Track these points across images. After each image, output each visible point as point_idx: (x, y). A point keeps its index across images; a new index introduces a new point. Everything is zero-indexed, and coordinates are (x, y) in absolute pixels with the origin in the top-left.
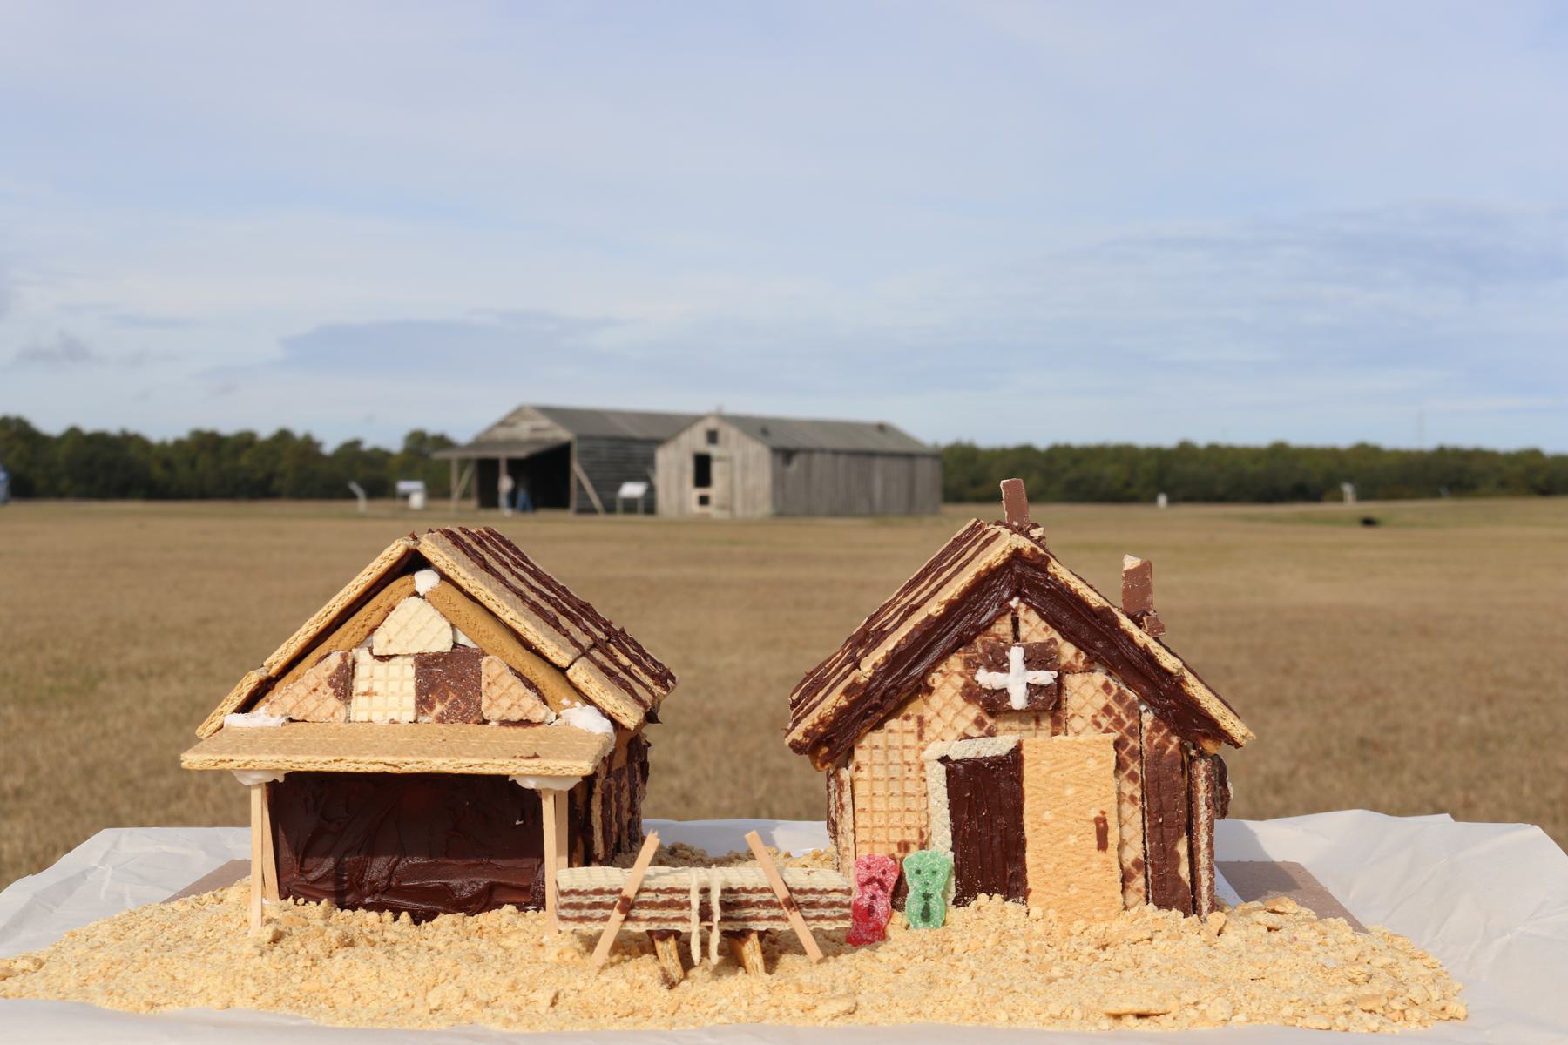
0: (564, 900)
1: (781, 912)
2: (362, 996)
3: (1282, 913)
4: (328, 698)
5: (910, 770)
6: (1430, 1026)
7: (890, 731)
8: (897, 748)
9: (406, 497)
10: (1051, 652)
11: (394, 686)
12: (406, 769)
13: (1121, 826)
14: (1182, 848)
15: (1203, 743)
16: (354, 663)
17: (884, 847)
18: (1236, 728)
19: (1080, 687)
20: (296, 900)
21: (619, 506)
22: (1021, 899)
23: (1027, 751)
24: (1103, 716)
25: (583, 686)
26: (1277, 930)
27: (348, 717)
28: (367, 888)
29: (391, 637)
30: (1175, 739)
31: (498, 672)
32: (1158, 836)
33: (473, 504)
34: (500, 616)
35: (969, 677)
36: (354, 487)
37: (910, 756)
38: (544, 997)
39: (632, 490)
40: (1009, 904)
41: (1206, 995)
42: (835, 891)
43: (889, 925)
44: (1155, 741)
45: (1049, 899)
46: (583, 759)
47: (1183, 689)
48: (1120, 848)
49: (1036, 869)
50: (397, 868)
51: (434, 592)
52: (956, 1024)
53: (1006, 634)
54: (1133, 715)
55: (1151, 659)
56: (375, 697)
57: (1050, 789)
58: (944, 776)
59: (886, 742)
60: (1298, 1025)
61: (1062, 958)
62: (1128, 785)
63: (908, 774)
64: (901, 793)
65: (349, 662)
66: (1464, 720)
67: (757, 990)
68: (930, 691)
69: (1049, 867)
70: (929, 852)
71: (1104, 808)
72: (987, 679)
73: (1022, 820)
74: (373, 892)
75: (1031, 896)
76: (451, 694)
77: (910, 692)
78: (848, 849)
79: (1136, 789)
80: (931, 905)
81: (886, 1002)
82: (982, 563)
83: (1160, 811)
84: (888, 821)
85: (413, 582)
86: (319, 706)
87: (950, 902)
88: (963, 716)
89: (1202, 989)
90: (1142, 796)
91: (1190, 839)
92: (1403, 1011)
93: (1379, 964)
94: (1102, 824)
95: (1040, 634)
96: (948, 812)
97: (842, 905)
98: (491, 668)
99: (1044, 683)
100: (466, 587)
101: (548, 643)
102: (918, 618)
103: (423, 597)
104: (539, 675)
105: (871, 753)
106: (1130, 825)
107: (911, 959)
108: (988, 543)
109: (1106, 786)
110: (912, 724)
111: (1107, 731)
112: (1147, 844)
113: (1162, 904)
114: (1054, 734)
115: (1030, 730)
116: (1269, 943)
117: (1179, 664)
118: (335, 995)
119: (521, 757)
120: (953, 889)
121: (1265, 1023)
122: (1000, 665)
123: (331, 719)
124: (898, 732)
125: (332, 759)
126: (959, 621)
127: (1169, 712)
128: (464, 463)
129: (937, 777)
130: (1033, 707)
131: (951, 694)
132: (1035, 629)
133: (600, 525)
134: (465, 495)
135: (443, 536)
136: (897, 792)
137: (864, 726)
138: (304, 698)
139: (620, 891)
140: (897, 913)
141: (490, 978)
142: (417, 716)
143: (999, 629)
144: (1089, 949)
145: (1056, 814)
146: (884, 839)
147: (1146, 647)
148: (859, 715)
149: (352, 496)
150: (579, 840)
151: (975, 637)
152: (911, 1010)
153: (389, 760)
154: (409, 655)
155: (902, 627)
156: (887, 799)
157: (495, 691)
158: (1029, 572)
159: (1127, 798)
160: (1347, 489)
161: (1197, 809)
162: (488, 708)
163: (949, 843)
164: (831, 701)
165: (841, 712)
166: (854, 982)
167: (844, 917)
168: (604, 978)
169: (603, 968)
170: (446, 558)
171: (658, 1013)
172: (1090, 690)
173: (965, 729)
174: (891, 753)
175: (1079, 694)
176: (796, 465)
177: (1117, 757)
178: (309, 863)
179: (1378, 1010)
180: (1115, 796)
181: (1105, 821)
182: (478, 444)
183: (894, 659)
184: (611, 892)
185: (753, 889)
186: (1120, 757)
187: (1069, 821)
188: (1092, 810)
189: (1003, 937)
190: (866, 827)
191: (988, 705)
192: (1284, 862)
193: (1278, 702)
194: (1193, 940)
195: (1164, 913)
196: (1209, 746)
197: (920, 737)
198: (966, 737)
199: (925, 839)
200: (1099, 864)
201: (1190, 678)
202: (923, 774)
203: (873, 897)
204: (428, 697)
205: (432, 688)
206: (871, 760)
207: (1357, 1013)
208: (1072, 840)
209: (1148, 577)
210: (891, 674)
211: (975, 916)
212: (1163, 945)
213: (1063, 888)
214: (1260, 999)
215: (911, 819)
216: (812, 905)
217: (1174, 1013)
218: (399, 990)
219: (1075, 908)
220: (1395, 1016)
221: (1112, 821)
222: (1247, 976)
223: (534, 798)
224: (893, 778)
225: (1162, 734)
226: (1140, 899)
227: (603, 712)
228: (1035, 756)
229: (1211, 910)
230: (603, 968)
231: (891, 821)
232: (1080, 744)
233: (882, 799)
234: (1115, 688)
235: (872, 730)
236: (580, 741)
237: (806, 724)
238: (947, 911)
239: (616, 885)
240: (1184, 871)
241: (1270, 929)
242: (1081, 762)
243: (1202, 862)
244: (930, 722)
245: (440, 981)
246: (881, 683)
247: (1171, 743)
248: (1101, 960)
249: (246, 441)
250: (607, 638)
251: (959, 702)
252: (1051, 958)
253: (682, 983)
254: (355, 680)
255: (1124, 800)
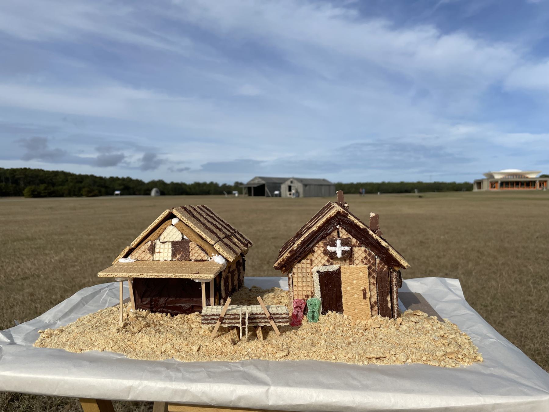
0: (203, 318)
1: (268, 320)
2: (144, 346)
3: (418, 315)
4: (148, 254)
5: (308, 274)
6: (472, 364)
7: (303, 263)
8: (305, 268)
9: (235, 194)
10: (349, 241)
11: (166, 250)
12: (161, 277)
13: (370, 292)
14: (389, 299)
15: (394, 268)
16: (155, 244)
17: (301, 296)
18: (405, 263)
19: (357, 251)
20: (140, 309)
21: (274, 195)
22: (341, 312)
23: (342, 270)
24: (365, 259)
25: (218, 250)
26: (418, 323)
27: (153, 259)
28: (159, 306)
29: (165, 237)
30: (386, 266)
31: (194, 246)
32: (381, 295)
33: (247, 195)
34: (195, 230)
35: (325, 248)
36: (225, 192)
37: (309, 270)
38: (195, 348)
39: (277, 192)
40: (337, 314)
41: (398, 352)
42: (284, 314)
43: (303, 320)
44: (380, 267)
45: (349, 313)
46: (211, 274)
47: (388, 252)
48: (370, 298)
49: (345, 304)
50: (167, 301)
51: (177, 224)
52: (319, 360)
53: (335, 236)
54: (373, 259)
55: (379, 243)
56: (161, 253)
57: (349, 281)
58: (318, 276)
59: (302, 266)
60: (428, 364)
61: (353, 334)
62: (372, 279)
63: (308, 276)
64: (306, 281)
65: (153, 244)
66: (442, 237)
67: (260, 346)
68: (314, 252)
69: (349, 303)
70: (314, 299)
71: (365, 287)
72: (329, 248)
73: (341, 289)
74: (161, 308)
75: (344, 312)
76: (181, 252)
77: (308, 252)
78: (291, 297)
79: (375, 281)
80: (315, 314)
81: (298, 352)
82: (328, 215)
83: (382, 287)
84: (302, 289)
85: (171, 221)
86: (145, 256)
87: (320, 313)
88: (323, 259)
89: (397, 349)
90: (377, 283)
91: (391, 296)
92: (462, 358)
93: (451, 337)
94: (365, 292)
95: (345, 236)
96: (319, 287)
97: (286, 318)
98: (192, 245)
99: (347, 250)
100: (185, 223)
101: (208, 238)
102: (310, 231)
103: (174, 226)
104: (206, 247)
105: (297, 269)
106: (373, 291)
107: (307, 333)
108: (331, 209)
109: (366, 280)
110: (309, 261)
111: (366, 264)
112: (378, 297)
113: (383, 315)
114: (350, 265)
115: (343, 263)
116: (416, 329)
117: (387, 244)
118: (136, 346)
119: (194, 273)
120: (321, 309)
121: (418, 363)
122: (334, 245)
123: (149, 260)
124: (304, 263)
125: (140, 274)
126: (322, 232)
127: (384, 259)
128: (245, 188)
129: (316, 277)
130: (344, 257)
131: (320, 253)
132: (344, 234)
133: (270, 199)
134: (246, 194)
135: (182, 208)
136: (305, 280)
137: (295, 262)
138: (141, 254)
139: (220, 315)
140: (305, 316)
141: (181, 341)
142: (172, 259)
143: (334, 234)
144: (361, 331)
145: (351, 288)
146: (301, 294)
147: (377, 240)
148: (294, 259)
149: (224, 194)
150: (217, 293)
151: (327, 236)
152: (305, 355)
153: (156, 274)
154: (170, 242)
155: (306, 233)
156: (302, 283)
157: (194, 252)
158: (342, 218)
159: (372, 284)
160: (416, 191)
161: (393, 287)
162: (191, 256)
163: (320, 296)
164: (286, 255)
165: (288, 258)
166: (289, 343)
167: (287, 322)
168: (215, 342)
169: (215, 337)
170: (180, 215)
171: (229, 354)
172: (360, 252)
173: (324, 263)
174: (303, 269)
175: (357, 253)
176: (308, 187)
177: (369, 272)
178: (144, 299)
179: (454, 358)
180: (368, 283)
181: (365, 290)
182: (248, 184)
183: (303, 243)
184: (217, 315)
185: (260, 313)
186: (370, 272)
187: (355, 290)
188: (362, 287)
189: (336, 326)
190: (296, 291)
191: (330, 256)
192: (415, 293)
193: (403, 233)
194: (393, 327)
195: (383, 318)
196: (397, 269)
197: (311, 265)
198: (324, 265)
199: (313, 294)
200: (364, 303)
201: (390, 249)
202: (312, 276)
203: (298, 312)
204: (175, 253)
205: (176, 251)
206: (297, 271)
207: (447, 359)
208: (356, 296)
209: (378, 219)
210: (303, 247)
211: (327, 318)
212: (384, 330)
213: (354, 310)
214: (415, 353)
215: (309, 289)
216: (277, 318)
217: (388, 358)
218: (154, 345)
219: (357, 316)
220: (459, 360)
221: (368, 290)
222: (410, 343)
223: (199, 284)
224: (304, 277)
225: (382, 265)
226: (376, 313)
227: (223, 257)
228: (344, 271)
229: (398, 317)
230: (215, 337)
231: (303, 289)
232: (358, 268)
233: (301, 282)
234: (368, 251)
235: (297, 263)
236: (214, 267)
237: (279, 261)
238: (319, 316)
239: (219, 313)
240: (389, 305)
241: (415, 323)
242: (358, 273)
243: (395, 302)
244: (314, 261)
245: (167, 342)
246: (300, 249)
247: (385, 267)
248: (365, 335)
249: (205, 184)
250: (231, 234)
251: (322, 255)
252: (349, 334)
253: (238, 343)
254: (155, 249)
255: (371, 284)
